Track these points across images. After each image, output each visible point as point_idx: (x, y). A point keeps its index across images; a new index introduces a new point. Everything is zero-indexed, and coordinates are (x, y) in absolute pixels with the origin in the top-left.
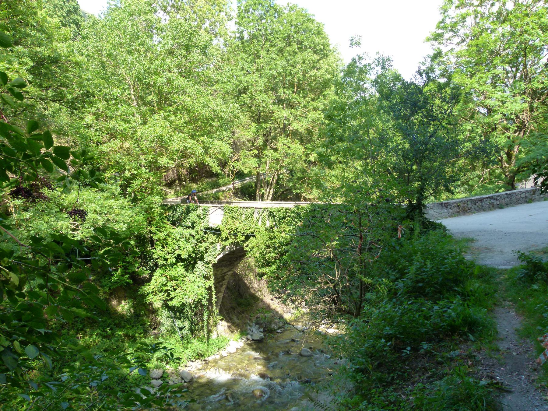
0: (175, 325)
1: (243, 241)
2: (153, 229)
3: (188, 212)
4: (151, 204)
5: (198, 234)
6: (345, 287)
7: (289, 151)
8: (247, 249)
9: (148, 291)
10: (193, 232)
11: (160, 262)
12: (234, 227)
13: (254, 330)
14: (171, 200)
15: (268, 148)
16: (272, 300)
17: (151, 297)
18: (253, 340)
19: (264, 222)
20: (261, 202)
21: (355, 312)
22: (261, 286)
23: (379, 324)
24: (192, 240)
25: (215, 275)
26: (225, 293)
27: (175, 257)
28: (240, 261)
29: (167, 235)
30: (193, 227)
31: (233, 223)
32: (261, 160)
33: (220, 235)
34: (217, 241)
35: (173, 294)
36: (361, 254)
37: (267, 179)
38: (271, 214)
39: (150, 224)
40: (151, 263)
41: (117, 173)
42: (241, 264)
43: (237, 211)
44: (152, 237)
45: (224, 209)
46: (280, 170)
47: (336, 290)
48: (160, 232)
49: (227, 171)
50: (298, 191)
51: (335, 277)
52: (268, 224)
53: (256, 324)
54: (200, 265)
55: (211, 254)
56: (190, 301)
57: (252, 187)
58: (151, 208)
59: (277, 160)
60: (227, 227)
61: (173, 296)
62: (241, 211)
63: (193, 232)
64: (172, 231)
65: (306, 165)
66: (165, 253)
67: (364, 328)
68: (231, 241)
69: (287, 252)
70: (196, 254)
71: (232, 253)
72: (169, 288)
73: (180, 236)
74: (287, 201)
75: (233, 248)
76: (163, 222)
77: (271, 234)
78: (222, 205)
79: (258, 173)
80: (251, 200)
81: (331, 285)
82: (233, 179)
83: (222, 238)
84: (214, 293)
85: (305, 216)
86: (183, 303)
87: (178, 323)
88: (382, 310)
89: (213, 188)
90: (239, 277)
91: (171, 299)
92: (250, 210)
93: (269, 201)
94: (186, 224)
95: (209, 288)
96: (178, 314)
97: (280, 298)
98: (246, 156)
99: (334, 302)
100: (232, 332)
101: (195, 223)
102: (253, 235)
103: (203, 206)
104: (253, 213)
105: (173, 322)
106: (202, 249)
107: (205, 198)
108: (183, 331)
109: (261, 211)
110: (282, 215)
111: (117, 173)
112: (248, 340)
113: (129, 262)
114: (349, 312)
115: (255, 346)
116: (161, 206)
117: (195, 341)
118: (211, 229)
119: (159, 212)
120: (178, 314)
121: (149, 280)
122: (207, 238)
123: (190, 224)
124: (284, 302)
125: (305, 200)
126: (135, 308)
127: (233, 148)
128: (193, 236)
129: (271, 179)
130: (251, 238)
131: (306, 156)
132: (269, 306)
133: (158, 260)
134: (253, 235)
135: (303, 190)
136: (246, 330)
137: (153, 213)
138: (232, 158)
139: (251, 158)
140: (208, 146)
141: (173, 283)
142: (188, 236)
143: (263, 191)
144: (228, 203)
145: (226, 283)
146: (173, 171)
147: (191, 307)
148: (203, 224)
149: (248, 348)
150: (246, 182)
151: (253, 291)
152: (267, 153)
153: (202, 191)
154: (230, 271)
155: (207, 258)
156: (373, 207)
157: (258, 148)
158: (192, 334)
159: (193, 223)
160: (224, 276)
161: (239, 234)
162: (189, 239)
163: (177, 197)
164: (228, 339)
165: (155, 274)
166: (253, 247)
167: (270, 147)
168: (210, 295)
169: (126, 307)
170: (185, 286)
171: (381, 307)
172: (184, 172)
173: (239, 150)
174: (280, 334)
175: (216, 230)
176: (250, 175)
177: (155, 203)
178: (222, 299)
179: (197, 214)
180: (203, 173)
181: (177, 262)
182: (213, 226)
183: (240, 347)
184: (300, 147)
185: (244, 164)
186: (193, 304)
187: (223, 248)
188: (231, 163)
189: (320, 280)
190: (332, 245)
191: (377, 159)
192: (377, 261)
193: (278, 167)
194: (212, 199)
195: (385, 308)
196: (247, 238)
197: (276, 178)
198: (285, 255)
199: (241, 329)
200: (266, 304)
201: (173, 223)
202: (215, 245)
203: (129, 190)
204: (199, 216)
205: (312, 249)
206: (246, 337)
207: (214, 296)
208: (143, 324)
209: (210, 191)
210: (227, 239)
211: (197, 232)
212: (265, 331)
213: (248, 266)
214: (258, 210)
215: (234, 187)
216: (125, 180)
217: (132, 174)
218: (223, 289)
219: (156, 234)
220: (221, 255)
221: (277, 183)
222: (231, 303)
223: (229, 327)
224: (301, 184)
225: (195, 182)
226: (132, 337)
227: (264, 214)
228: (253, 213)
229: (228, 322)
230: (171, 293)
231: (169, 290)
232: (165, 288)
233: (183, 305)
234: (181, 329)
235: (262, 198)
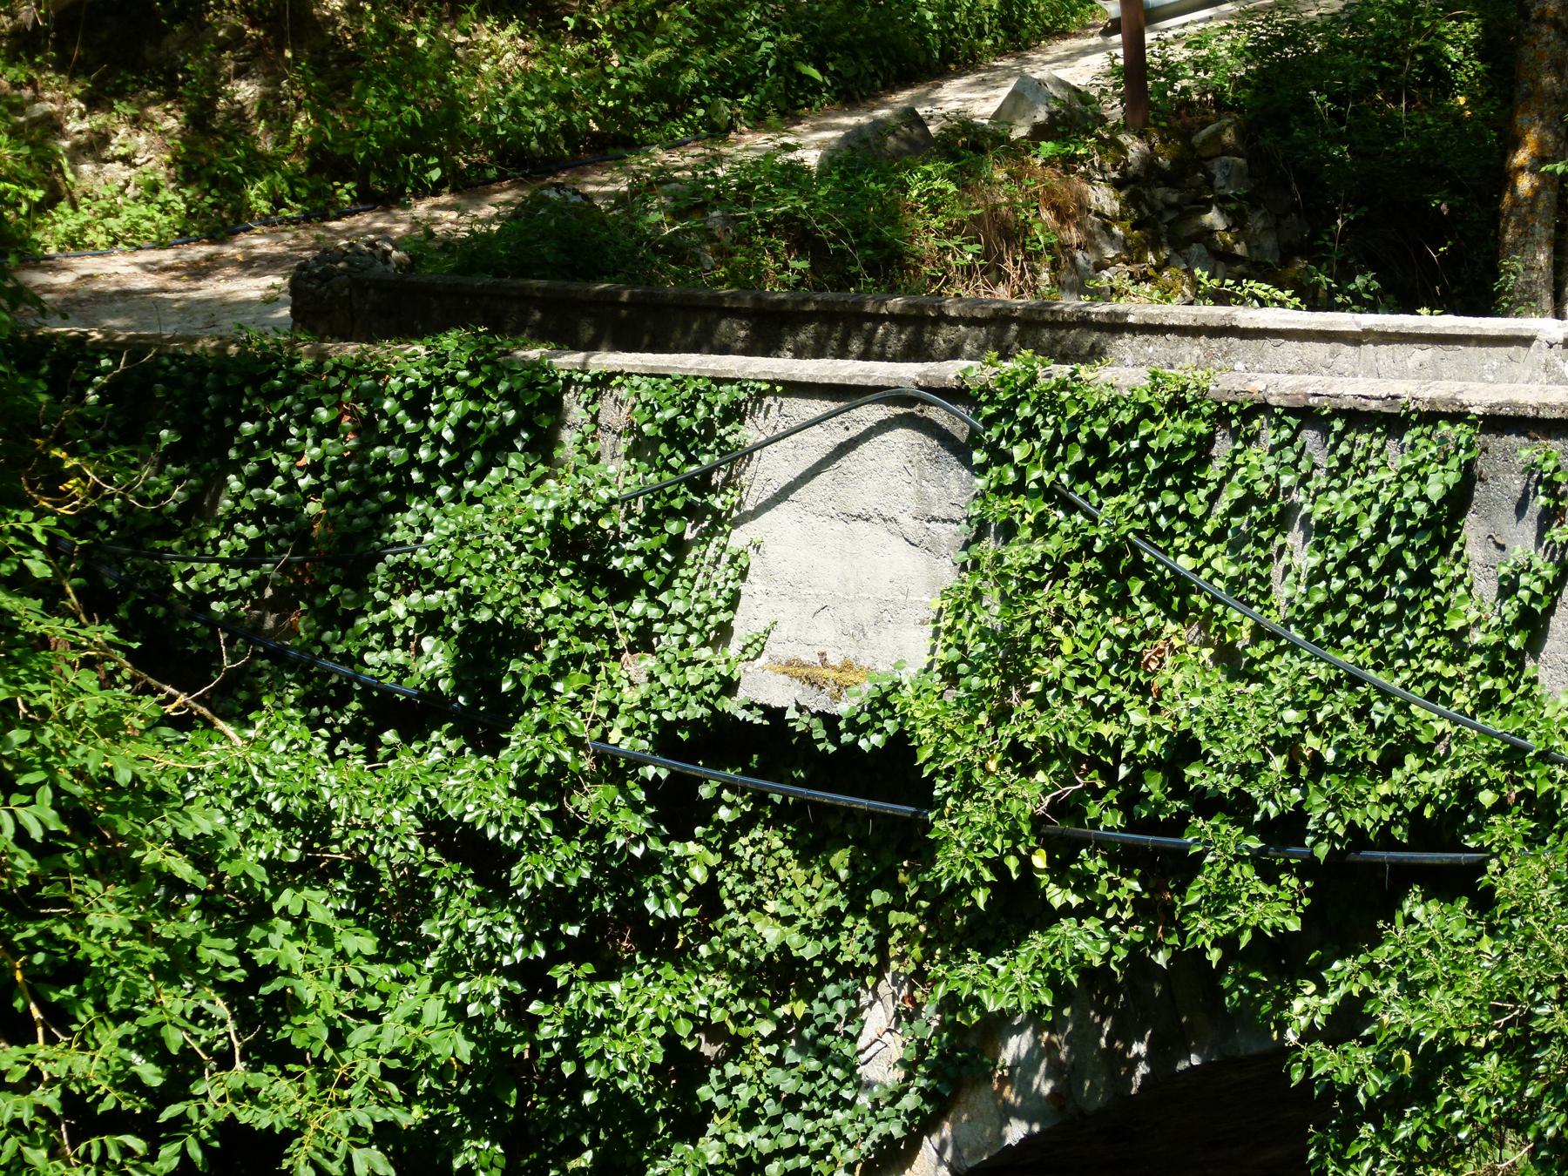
5: (567, 826)
31: (1126, 655)
62: (1259, 462)
73: (273, 842)
75: (1118, 1063)
83: (943, 901)
101: (525, 641)
104: (1459, 500)
107: (676, 251)
122: (707, 897)
130: (1413, 905)
148: (639, 666)
179: (543, 503)
202: (831, 1004)
209: (751, 144)
214: (1525, 450)
215: (1134, 71)
228: (1459, 500)
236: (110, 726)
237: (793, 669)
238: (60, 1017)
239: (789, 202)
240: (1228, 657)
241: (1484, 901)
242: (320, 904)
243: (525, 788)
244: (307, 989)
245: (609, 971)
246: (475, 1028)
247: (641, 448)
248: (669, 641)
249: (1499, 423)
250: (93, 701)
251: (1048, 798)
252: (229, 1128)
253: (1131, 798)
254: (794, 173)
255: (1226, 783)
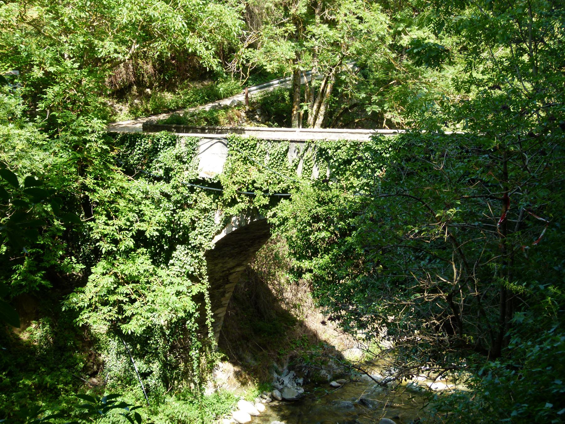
0: (133, 369)
1: (266, 207)
2: (89, 181)
3: (155, 151)
4: (84, 133)
6: (468, 301)
7: (360, 27)
8: (275, 221)
9: (81, 304)
10: (167, 188)
11: (105, 247)
12: (248, 179)
13: (286, 381)
14: (124, 123)
15: (318, 19)
16: (324, 323)
17: (86, 316)
18: (283, 400)
19: (308, 170)
20: (301, 129)
21: (489, 348)
22: (299, 295)
23: (540, 372)
24: (165, 203)
25: (210, 273)
26: (228, 308)
27: (132, 237)
28: (260, 246)
29: (117, 193)
30: (167, 179)
31: (247, 170)
32: (302, 45)
33: (221, 194)
34: (214, 207)
35: (129, 310)
36: (505, 233)
37: (314, 84)
38: (322, 154)
39: (82, 172)
40: (86, 249)
41: (16, 69)
42: (262, 253)
43: (254, 147)
44: (87, 197)
45: (228, 143)
46: (341, 64)
47: (452, 305)
48: (103, 186)
49: (233, 66)
50: (376, 109)
51: (451, 279)
52: (316, 174)
53: (290, 369)
54: (180, 251)
55: (202, 231)
56: (162, 322)
57: (284, 99)
58: (85, 142)
59: (336, 44)
60: (235, 179)
61: (128, 313)
62: (262, 146)
63: (167, 188)
64: (125, 185)
65: (394, 55)
66: (113, 228)
67: (508, 379)
68: (242, 206)
69: (355, 229)
70: (173, 231)
71: (243, 230)
72: (121, 298)
73: (141, 195)
74: (357, 127)
75: (246, 220)
76: (107, 168)
77: (323, 194)
78: (224, 135)
79: (297, 73)
80: (280, 126)
81: (444, 295)
82: (246, 83)
83: (224, 201)
84: (208, 307)
85: (393, 158)
86: (148, 327)
87: (139, 365)
88: (547, 346)
89: (206, 102)
90: (256, 278)
91: (127, 320)
92: (279, 145)
93: (317, 128)
94: (154, 173)
95: (198, 298)
96: (138, 346)
97: (338, 318)
98: (271, 37)
99: (448, 328)
100: (244, 384)
101: (172, 170)
102: (285, 194)
103: (185, 137)
104: (287, 151)
105: (131, 363)
106: (186, 221)
108: (149, 379)
109: (302, 147)
110: (344, 156)
111: (16, 69)
112: (273, 398)
113: (43, 247)
114: (480, 349)
115: (286, 411)
116: (104, 136)
117: (171, 400)
118: (202, 182)
119: (99, 151)
120: (138, 346)
121: (83, 282)
122: (196, 201)
123: (161, 172)
124: (346, 329)
125: (391, 125)
126: (56, 334)
127: (245, 20)
128: (167, 196)
129: (323, 83)
130: (282, 200)
131: (394, 37)
132: (315, 335)
133: (101, 243)
134: (285, 194)
135: (386, 106)
136: (270, 381)
137: (88, 150)
138: (243, 40)
139: (282, 40)
140: (195, 14)
141: (127, 289)
142: (157, 196)
143: (305, 108)
144: (235, 130)
145: (232, 290)
146: (126, 67)
147: (164, 334)
148: (186, 172)
149: (274, 414)
150: (271, 89)
151: (284, 306)
152: (314, 31)
153: (184, 107)
154: (239, 265)
155: (195, 238)
156: (532, 140)
157: (296, 20)
158: (167, 386)
159: (168, 170)
160: (227, 276)
161: (258, 193)
162: (159, 201)
163: (136, 119)
164: (236, 397)
165: (93, 270)
166: (286, 219)
167: (322, 18)
168: (202, 310)
169: (38, 334)
170: (152, 294)
171: (545, 340)
172: (149, 67)
173: (258, 25)
174: (339, 390)
175: (213, 185)
176: (279, 74)
177: (93, 132)
178: (225, 321)
180: (187, 71)
181: (137, 246)
182: (207, 177)
183: (258, 413)
184: (384, 18)
185: (268, 52)
186: (168, 328)
187: (227, 221)
188: (243, 52)
189: (423, 284)
190: (448, 216)
191: (542, 41)
192: (537, 250)
193: (338, 59)
194: (204, 124)
195: (554, 341)
196: (275, 200)
197: (332, 81)
198: (350, 235)
199: (260, 378)
200: (310, 331)
201: (129, 171)
202: (211, 214)
203: (41, 105)
204: (179, 158)
205: (406, 223)
206: (269, 394)
207: (209, 313)
208: (71, 366)
209: (201, 108)
210: (234, 202)
211: (175, 187)
212: (308, 383)
213: (276, 256)
214: (295, 144)
216: (33, 84)
217: (47, 73)
218: (226, 300)
219: (94, 191)
220: (223, 234)
221: (334, 91)
222: (240, 329)
223: (237, 375)
224: (382, 94)
225: (171, 88)
226: (51, 391)
227: (308, 154)
228: (287, 151)
229: (235, 364)
230: (125, 307)
231: (122, 302)
232: (112, 298)
233: (149, 331)
234: (145, 375)
235: (304, 122)
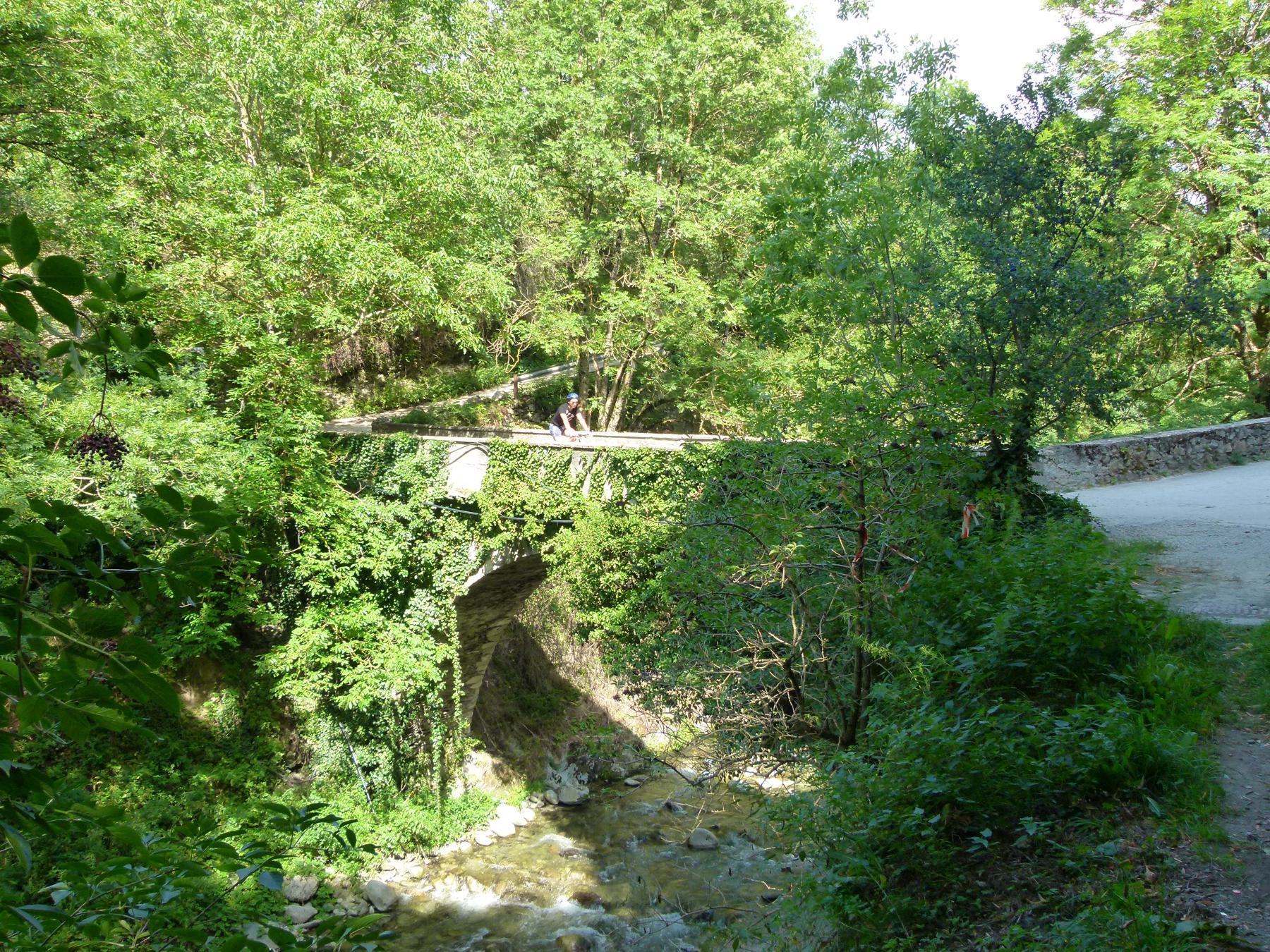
5: (419, 517)
31: (514, 487)
62: (536, 455)
73: (368, 520)
83: (482, 529)
101: (411, 485)
107: (438, 419)
122: (443, 529)
130: (562, 529)
148: (431, 489)
209: (452, 402)
228: (569, 461)
236: (340, 498)
237: (457, 490)
238: (333, 548)
239: (458, 411)
240: (531, 488)
241: (573, 528)
242: (376, 530)
243: (411, 510)
244: (374, 545)
245: (426, 541)
246: (403, 551)
247: (432, 452)
248: (436, 485)
249: (576, 449)
250: (339, 494)
251: (1009, 803)
252: (363, 569)
253: (515, 512)
254: (458, 407)
255: (531, 509)
